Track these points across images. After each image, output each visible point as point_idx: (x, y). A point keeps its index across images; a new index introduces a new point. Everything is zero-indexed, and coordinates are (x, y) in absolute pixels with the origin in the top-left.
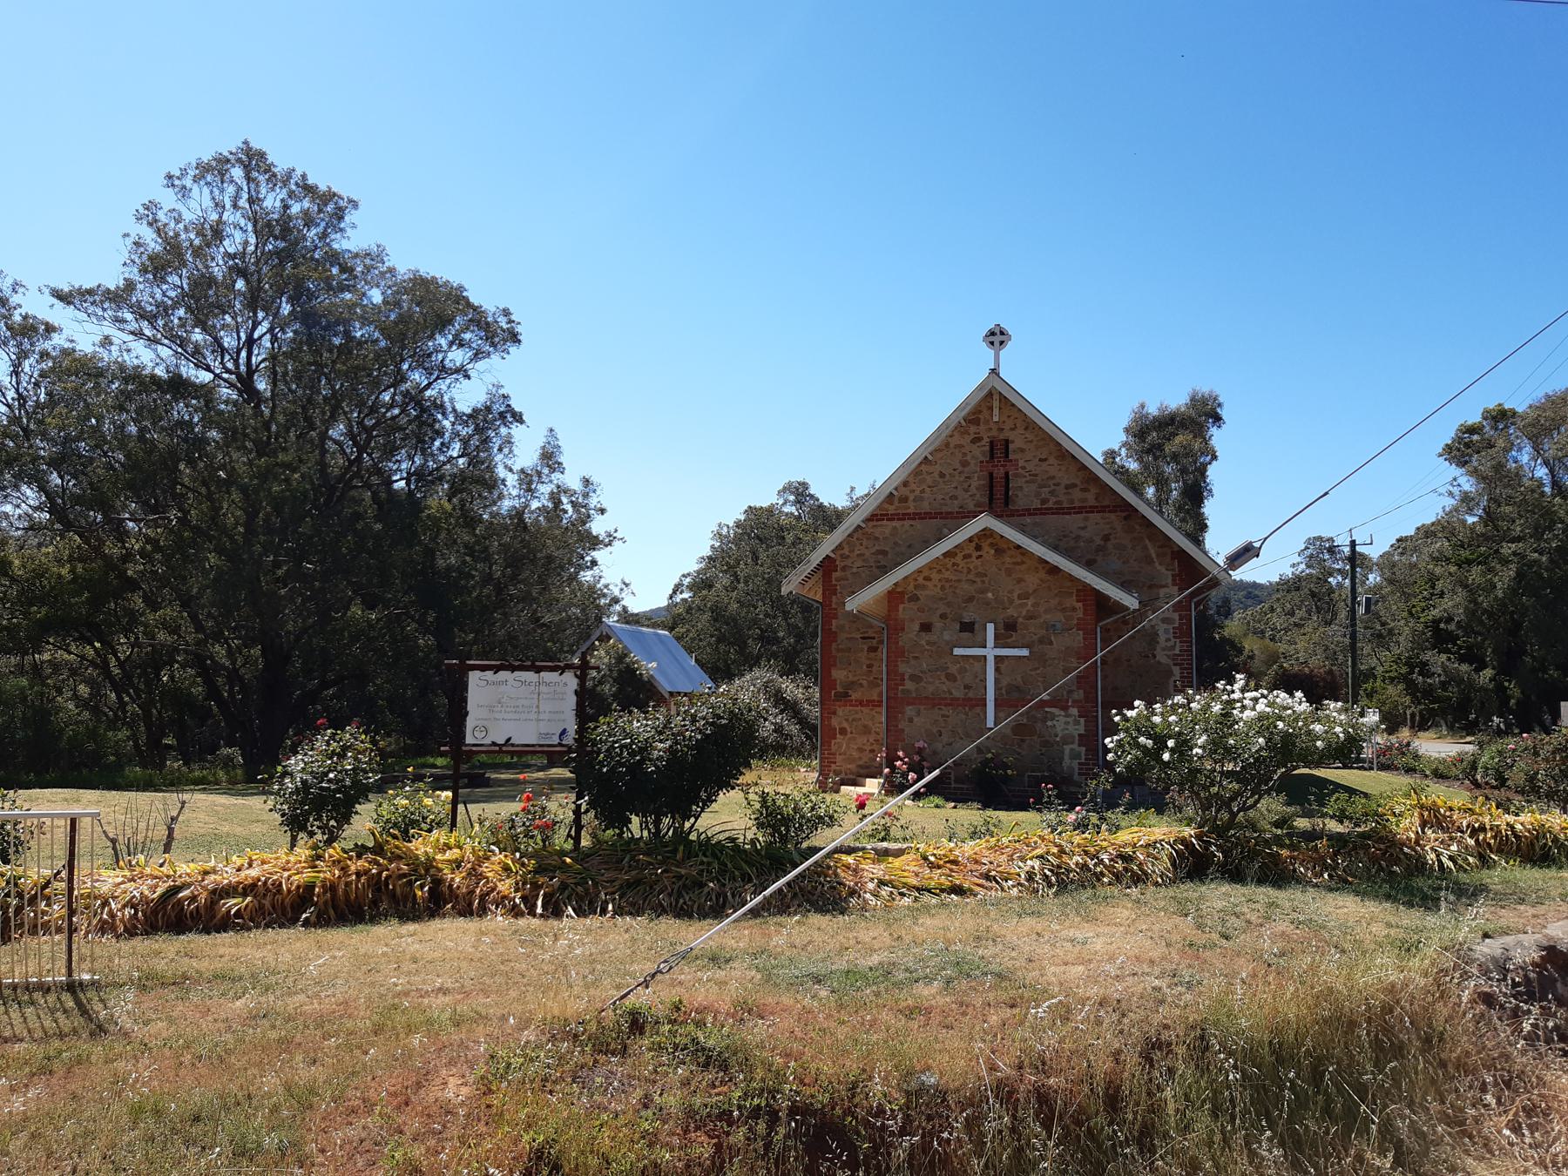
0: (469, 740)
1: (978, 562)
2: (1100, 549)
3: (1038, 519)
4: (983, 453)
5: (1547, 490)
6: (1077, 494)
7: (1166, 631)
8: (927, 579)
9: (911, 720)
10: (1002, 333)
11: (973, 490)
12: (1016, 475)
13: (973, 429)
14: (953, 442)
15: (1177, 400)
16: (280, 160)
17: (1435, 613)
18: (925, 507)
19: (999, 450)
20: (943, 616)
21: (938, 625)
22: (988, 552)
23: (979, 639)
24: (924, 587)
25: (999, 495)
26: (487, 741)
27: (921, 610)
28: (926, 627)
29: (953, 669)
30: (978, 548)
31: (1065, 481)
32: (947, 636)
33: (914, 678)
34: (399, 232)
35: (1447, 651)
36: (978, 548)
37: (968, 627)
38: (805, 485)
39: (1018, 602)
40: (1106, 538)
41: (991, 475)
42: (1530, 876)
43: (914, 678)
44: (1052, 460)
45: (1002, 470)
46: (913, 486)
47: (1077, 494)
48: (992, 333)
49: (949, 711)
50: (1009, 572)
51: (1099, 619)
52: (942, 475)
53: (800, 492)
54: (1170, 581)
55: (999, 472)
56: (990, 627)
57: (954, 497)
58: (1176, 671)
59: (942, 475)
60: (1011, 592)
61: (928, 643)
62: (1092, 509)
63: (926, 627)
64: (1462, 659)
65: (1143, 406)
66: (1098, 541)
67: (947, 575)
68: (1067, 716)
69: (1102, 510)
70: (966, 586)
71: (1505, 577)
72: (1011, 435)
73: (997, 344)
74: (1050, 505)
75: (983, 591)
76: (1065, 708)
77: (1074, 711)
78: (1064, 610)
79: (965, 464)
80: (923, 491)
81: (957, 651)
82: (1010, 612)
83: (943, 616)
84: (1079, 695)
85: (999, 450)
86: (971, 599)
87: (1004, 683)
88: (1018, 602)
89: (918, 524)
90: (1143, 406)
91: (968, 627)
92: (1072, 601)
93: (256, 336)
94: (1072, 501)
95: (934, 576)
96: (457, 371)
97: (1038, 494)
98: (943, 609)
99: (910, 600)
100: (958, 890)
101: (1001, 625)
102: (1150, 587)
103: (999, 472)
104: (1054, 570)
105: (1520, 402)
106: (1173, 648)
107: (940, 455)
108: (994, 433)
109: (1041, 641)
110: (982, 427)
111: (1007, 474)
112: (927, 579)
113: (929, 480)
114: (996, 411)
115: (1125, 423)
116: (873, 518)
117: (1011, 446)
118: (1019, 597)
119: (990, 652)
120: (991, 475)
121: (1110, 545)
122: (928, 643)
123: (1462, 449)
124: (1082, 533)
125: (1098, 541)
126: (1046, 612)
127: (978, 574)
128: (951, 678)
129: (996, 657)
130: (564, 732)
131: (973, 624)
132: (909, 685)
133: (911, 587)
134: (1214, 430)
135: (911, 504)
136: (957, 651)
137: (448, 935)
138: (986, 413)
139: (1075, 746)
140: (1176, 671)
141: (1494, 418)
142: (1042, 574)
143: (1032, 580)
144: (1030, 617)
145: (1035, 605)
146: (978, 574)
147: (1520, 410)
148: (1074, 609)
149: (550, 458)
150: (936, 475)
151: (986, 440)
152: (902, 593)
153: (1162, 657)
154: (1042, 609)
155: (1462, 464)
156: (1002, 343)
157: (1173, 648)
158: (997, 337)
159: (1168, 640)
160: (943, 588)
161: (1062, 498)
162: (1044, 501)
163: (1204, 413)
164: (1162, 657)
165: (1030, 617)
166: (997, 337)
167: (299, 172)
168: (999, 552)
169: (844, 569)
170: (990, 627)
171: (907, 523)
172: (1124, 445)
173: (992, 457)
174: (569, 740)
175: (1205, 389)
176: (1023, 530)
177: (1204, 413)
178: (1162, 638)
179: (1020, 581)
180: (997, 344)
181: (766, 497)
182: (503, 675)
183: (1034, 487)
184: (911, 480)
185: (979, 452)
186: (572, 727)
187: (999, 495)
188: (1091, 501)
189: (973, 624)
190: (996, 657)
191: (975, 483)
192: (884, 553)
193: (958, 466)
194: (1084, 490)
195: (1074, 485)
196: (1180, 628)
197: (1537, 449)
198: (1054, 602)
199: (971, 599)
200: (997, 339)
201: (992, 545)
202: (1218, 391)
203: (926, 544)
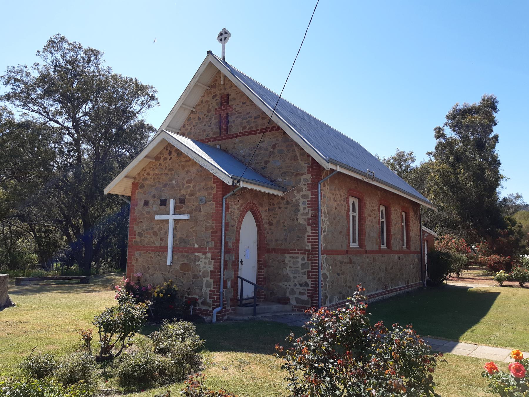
1: (170, 162)
2: (272, 153)
3: (241, 139)
4: (217, 104)
7: (304, 203)
9: (137, 260)
10: (226, 33)
12: (232, 114)
13: (213, 90)
14: (205, 99)
15: (476, 101)
19: (225, 100)
28: (146, 203)
33: (140, 234)
39: (186, 185)
40: (274, 147)
43: (140, 234)
45: (225, 113)
46: (187, 127)
48: (221, 34)
49: (152, 254)
50: (183, 167)
51: (224, 195)
54: (306, 171)
55: (224, 113)
56: (172, 202)
57: (204, 131)
59: (199, 119)
60: (183, 179)
61: (147, 213)
65: (457, 105)
66: (271, 150)
67: (157, 171)
68: (206, 258)
70: (163, 177)
73: (223, 40)
74: (247, 130)
75: (171, 180)
76: (205, 253)
77: (209, 255)
78: (207, 189)
79: (209, 111)
80: (191, 129)
81: (157, 217)
82: (183, 192)
84: (212, 244)
87: (178, 236)
88: (186, 185)
90: (457, 105)
94: (257, 126)
101: (178, 201)
102: (297, 175)
106: (307, 214)
107: (198, 107)
108: (222, 91)
110: (217, 89)
111: (227, 114)
115: (447, 113)
117: (230, 97)
118: (187, 183)
121: (276, 151)
124: (262, 145)
125: (271, 150)
126: (199, 190)
128: (155, 234)
129: (167, 221)
132: (138, 239)
134: (494, 114)
136: (157, 217)
139: (208, 279)
140: (309, 228)
144: (192, 195)
145: (194, 187)
148: (212, 188)
150: (196, 119)
153: (301, 221)
154: (197, 189)
156: (225, 38)
157: (307, 214)
159: (304, 209)
160: (154, 179)
161: (253, 125)
162: (244, 128)
163: (489, 106)
164: (301, 221)
165: (192, 195)
166: (223, 36)
167: (77, 43)
170: (172, 202)
172: (447, 124)
175: (489, 95)
177: (489, 106)
178: (301, 207)
180: (223, 40)
183: (239, 120)
184: (186, 123)
185: (214, 103)
190: (175, 221)
191: (214, 121)
193: (206, 112)
196: (311, 201)
199: (165, 185)
200: (223, 37)
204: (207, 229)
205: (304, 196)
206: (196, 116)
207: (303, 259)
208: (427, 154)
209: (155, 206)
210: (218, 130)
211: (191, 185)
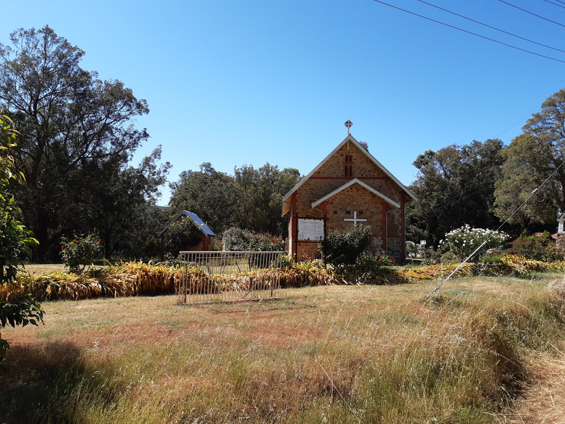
0: (299, 239)
5: (443, 177)
6: (372, 173)
8: (336, 197)
11: (341, 171)
13: (341, 152)
16: (59, 33)
17: (411, 214)
18: (326, 175)
19: (348, 159)
20: (340, 209)
21: (339, 212)
22: (354, 190)
23: (351, 216)
24: (335, 200)
25: (349, 173)
26: (303, 239)
27: (334, 207)
28: (335, 212)
29: (344, 225)
30: (351, 188)
31: (369, 169)
32: (342, 215)
34: (101, 66)
35: (414, 225)
36: (351, 188)
37: (348, 212)
38: (209, 164)
41: (346, 166)
42: (539, 274)
44: (364, 163)
47: (372, 173)
48: (347, 123)
50: (361, 196)
52: (331, 166)
53: (207, 166)
56: (355, 213)
58: (400, 226)
61: (336, 217)
62: (376, 178)
63: (335, 212)
64: (419, 228)
67: (342, 196)
69: (379, 178)
71: (433, 204)
72: (353, 154)
75: (353, 202)
76: (377, 237)
77: (380, 238)
78: (377, 208)
79: (338, 162)
81: (345, 220)
82: (361, 208)
83: (340, 209)
84: (381, 233)
85: (348, 159)
86: (349, 204)
89: (323, 180)
91: (348, 212)
92: (379, 205)
93: (39, 98)
94: (370, 175)
95: (338, 197)
96: (124, 118)
97: (360, 173)
98: (341, 207)
99: (330, 204)
100: (427, 279)
103: (349, 165)
104: (374, 195)
105: (435, 150)
108: (347, 153)
109: (370, 217)
110: (344, 151)
112: (336, 197)
113: (327, 167)
114: (348, 147)
116: (312, 178)
117: (352, 158)
119: (355, 220)
120: (346, 166)
122: (336, 217)
123: (419, 163)
127: (351, 197)
130: (321, 237)
131: (349, 212)
133: (331, 200)
135: (321, 174)
136: (345, 220)
137: (319, 290)
138: (345, 147)
140: (400, 226)
141: (428, 154)
142: (370, 197)
143: (368, 199)
145: (368, 206)
146: (351, 197)
147: (435, 152)
149: (157, 153)
151: (344, 156)
152: (328, 202)
153: (396, 223)
155: (419, 167)
158: (348, 124)
160: (340, 200)
162: (362, 175)
164: (396, 223)
166: (348, 124)
168: (358, 190)
169: (300, 194)
170: (355, 213)
171: (320, 180)
173: (346, 160)
174: (323, 239)
176: (368, 184)
178: (396, 217)
179: (364, 199)
181: (196, 169)
182: (307, 220)
183: (359, 170)
185: (342, 159)
186: (323, 235)
187: (349, 173)
188: (376, 176)
189: (349, 212)
191: (341, 168)
192: (313, 189)
194: (374, 172)
195: (371, 171)
197: (441, 165)
198: (374, 205)
199: (349, 204)
200: (349, 124)
201: (355, 188)
202: (367, 142)
203: (336, 188)
204: (377, 226)
205: (397, 212)
206: (330, 163)
207: (397, 240)
208: (147, 111)
209: (341, 214)
210: (344, 174)
211: (367, 205)
